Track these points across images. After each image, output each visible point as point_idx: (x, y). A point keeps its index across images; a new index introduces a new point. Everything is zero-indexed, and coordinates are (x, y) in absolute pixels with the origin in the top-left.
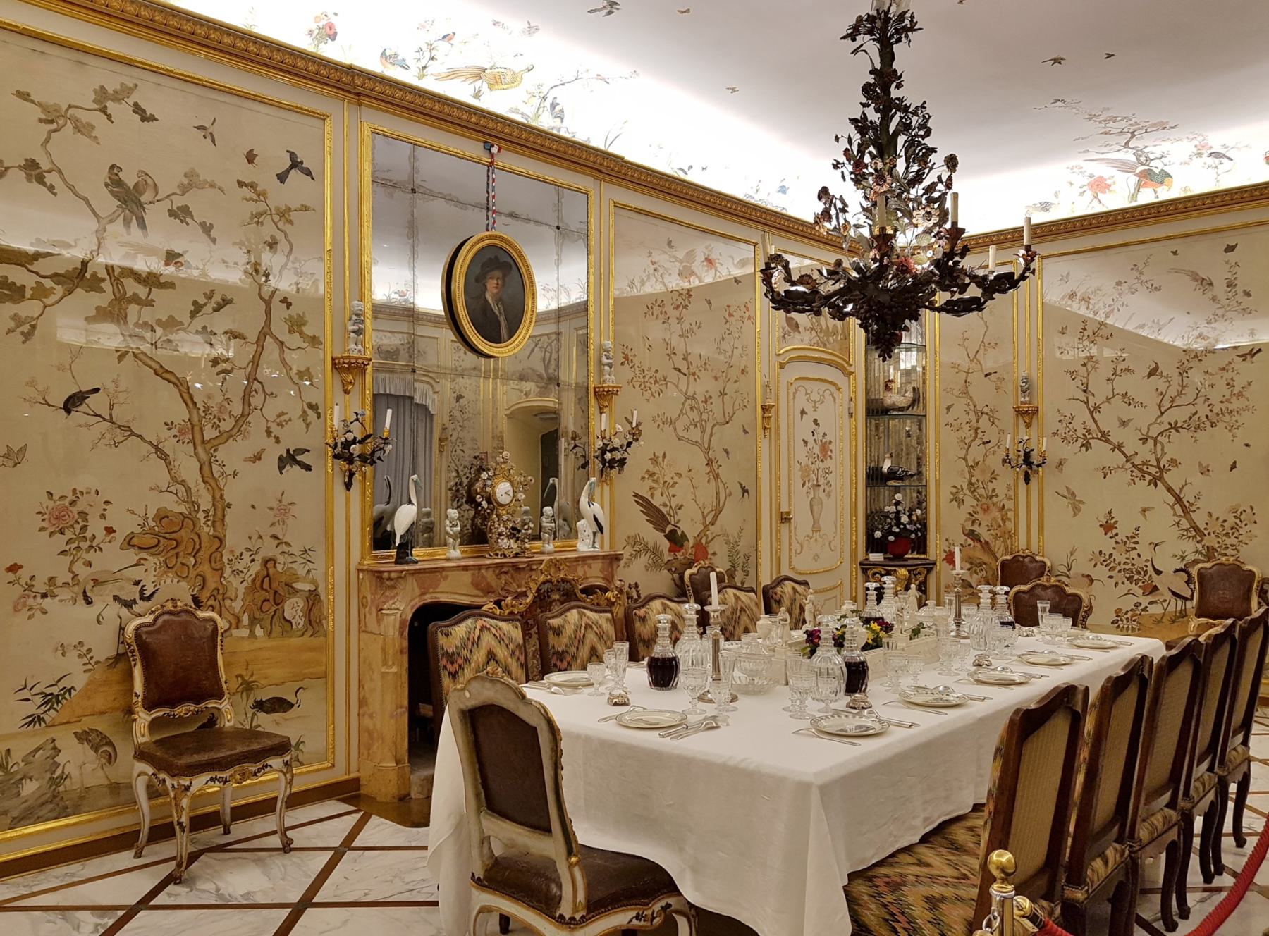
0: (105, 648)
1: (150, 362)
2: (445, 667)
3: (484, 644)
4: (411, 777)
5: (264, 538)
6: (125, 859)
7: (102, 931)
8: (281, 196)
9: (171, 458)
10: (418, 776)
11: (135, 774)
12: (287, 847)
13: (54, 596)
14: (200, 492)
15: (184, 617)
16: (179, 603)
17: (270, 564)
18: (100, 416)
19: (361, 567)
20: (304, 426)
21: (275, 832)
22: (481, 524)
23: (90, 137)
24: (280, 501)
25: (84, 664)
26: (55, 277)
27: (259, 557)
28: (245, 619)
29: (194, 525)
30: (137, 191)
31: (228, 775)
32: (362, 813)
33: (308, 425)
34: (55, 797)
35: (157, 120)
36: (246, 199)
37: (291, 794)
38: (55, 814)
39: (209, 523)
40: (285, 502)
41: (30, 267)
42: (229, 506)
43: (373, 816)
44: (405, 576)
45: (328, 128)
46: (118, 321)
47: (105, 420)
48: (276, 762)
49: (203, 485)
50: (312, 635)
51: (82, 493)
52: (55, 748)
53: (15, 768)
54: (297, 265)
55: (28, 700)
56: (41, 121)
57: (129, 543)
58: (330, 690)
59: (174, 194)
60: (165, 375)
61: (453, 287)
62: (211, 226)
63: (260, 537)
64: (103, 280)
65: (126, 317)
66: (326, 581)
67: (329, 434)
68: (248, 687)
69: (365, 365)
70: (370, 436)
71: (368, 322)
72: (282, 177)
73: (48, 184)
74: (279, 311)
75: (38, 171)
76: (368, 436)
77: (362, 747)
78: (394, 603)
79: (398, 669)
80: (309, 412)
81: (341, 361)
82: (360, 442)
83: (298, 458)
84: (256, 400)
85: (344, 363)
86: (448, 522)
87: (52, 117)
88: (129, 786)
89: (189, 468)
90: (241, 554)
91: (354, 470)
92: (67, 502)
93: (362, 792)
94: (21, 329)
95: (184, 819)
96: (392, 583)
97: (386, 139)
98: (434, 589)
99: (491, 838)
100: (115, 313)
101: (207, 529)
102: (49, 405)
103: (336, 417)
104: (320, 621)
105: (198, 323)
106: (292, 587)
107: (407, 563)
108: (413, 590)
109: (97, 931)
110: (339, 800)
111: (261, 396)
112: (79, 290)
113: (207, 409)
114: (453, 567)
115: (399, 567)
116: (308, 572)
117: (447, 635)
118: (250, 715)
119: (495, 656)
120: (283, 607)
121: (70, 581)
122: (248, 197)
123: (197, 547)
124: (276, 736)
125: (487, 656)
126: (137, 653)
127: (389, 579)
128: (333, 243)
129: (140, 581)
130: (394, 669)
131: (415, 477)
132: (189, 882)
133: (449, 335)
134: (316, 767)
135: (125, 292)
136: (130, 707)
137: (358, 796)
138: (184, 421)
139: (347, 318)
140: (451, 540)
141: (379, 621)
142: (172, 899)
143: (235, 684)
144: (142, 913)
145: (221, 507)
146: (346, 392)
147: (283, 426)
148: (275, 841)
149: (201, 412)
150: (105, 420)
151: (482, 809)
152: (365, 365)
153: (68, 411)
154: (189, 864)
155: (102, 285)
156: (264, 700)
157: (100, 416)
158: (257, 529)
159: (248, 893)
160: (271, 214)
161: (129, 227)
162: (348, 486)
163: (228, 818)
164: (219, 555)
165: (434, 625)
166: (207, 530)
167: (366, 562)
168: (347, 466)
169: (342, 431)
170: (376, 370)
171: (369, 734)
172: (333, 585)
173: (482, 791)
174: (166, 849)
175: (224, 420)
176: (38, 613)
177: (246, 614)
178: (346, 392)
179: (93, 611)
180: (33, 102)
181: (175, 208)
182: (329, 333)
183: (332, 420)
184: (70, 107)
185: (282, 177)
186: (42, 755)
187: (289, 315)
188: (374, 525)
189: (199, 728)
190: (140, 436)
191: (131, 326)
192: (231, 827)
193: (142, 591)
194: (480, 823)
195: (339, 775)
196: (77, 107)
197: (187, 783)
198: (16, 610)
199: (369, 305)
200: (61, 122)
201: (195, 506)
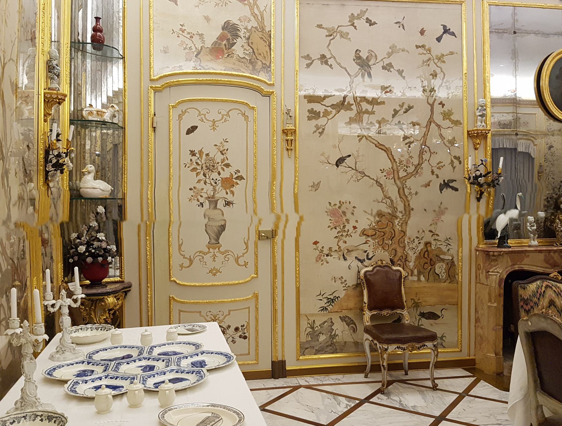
0: (352, 281)
1: (374, 141)
2: (522, 307)
3: (547, 296)
4: (504, 364)
5: (425, 232)
6: (360, 377)
7: (349, 408)
8: (438, 49)
9: (384, 186)
10: (506, 364)
11: (365, 339)
12: (435, 388)
13: (331, 256)
14: (398, 202)
15: (386, 269)
16: (384, 262)
17: (428, 245)
18: (351, 168)
19: (477, 249)
20: (452, 168)
21: (429, 379)
22: (550, 225)
23: (347, 39)
24: (440, 207)
25: (344, 287)
26: (332, 106)
27: (423, 242)
28: (416, 272)
29: (393, 225)
30: (368, 60)
31: (405, 347)
32: (476, 378)
33: (454, 168)
34: (332, 343)
35: (377, 24)
36: (420, 54)
37: (437, 361)
38: (332, 351)
39: (400, 224)
40: (442, 207)
41: (322, 103)
42: (412, 209)
43: (482, 381)
44: (503, 254)
45: (463, 8)
46: (359, 122)
47: (353, 169)
48: (429, 344)
49: (399, 199)
50: (450, 283)
51: (343, 203)
52: (332, 322)
53: (317, 329)
54: (447, 84)
55: (321, 300)
56: (327, 36)
57: (363, 233)
58: (459, 311)
59: (385, 58)
60: (380, 147)
61: (541, 84)
62: (403, 70)
63: (424, 231)
64: (352, 104)
65: (362, 121)
66: (458, 255)
67: (466, 172)
68: (416, 305)
69: (487, 133)
70: (490, 172)
71: (488, 110)
72: (439, 39)
73: (330, 64)
74: (438, 109)
75: (325, 59)
76: (489, 173)
77: (477, 344)
78: (496, 269)
79: (497, 305)
80: (455, 161)
81: (473, 132)
82: (484, 176)
83: (451, 184)
84: (426, 156)
85: (474, 133)
86: (528, 224)
87: (331, 34)
88: (362, 344)
89: (393, 192)
90: (414, 240)
91: (483, 190)
92: (337, 207)
93: (476, 366)
94: (318, 131)
95: (385, 364)
96: (495, 258)
97: (497, 7)
98: (520, 262)
99: (543, 406)
100: (357, 119)
101: (398, 227)
102: (330, 164)
103: (470, 163)
104: (454, 276)
105: (396, 120)
106: (440, 257)
107: (505, 247)
108: (507, 262)
109: (347, 407)
110: (462, 368)
111: (429, 154)
112: (342, 111)
113: (401, 162)
114: (533, 250)
115: (499, 250)
116: (448, 250)
117: (524, 289)
118: (418, 319)
119: (554, 303)
120: (435, 267)
121: (338, 250)
122: (421, 53)
123: (393, 235)
124: (429, 331)
125: (549, 303)
126: (365, 284)
127: (494, 256)
128: (467, 69)
129: (367, 251)
130: (495, 305)
131: (520, 194)
132: (388, 394)
133: (539, 112)
134: (452, 350)
135: (362, 109)
136: (362, 308)
137: (474, 369)
138: (389, 168)
139: (476, 108)
140: (532, 235)
141: (487, 277)
142: (380, 400)
143: (410, 303)
144: (366, 404)
145: (408, 210)
146: (476, 149)
147: (440, 169)
148: (429, 383)
149: (398, 163)
150: (353, 169)
151: (538, 389)
152: (487, 133)
153: (338, 166)
154: (387, 387)
155: (352, 107)
156: (425, 312)
157: (351, 168)
158: (422, 227)
159: (415, 406)
160: (433, 60)
161: (364, 78)
162: (479, 199)
163: (407, 368)
164: (403, 240)
165: (516, 283)
166: (398, 227)
167: (480, 246)
168: (479, 188)
169: (473, 170)
170: (493, 135)
171: (481, 337)
172: (462, 257)
173: (538, 379)
174: (377, 376)
175: (409, 167)
176: (325, 263)
177: (416, 269)
178: (476, 149)
179: (347, 263)
180: (323, 28)
181: (385, 65)
182: (465, 118)
183: (468, 164)
184: (339, 27)
185: (439, 39)
186: (327, 325)
187: (444, 111)
188: (485, 225)
189: (393, 322)
190: (369, 176)
191: (365, 125)
192: (408, 372)
193: (367, 255)
194: (536, 396)
195: (464, 356)
196: (341, 26)
197: (386, 347)
198: (317, 261)
199: (489, 100)
200: (335, 34)
201: (395, 209)
